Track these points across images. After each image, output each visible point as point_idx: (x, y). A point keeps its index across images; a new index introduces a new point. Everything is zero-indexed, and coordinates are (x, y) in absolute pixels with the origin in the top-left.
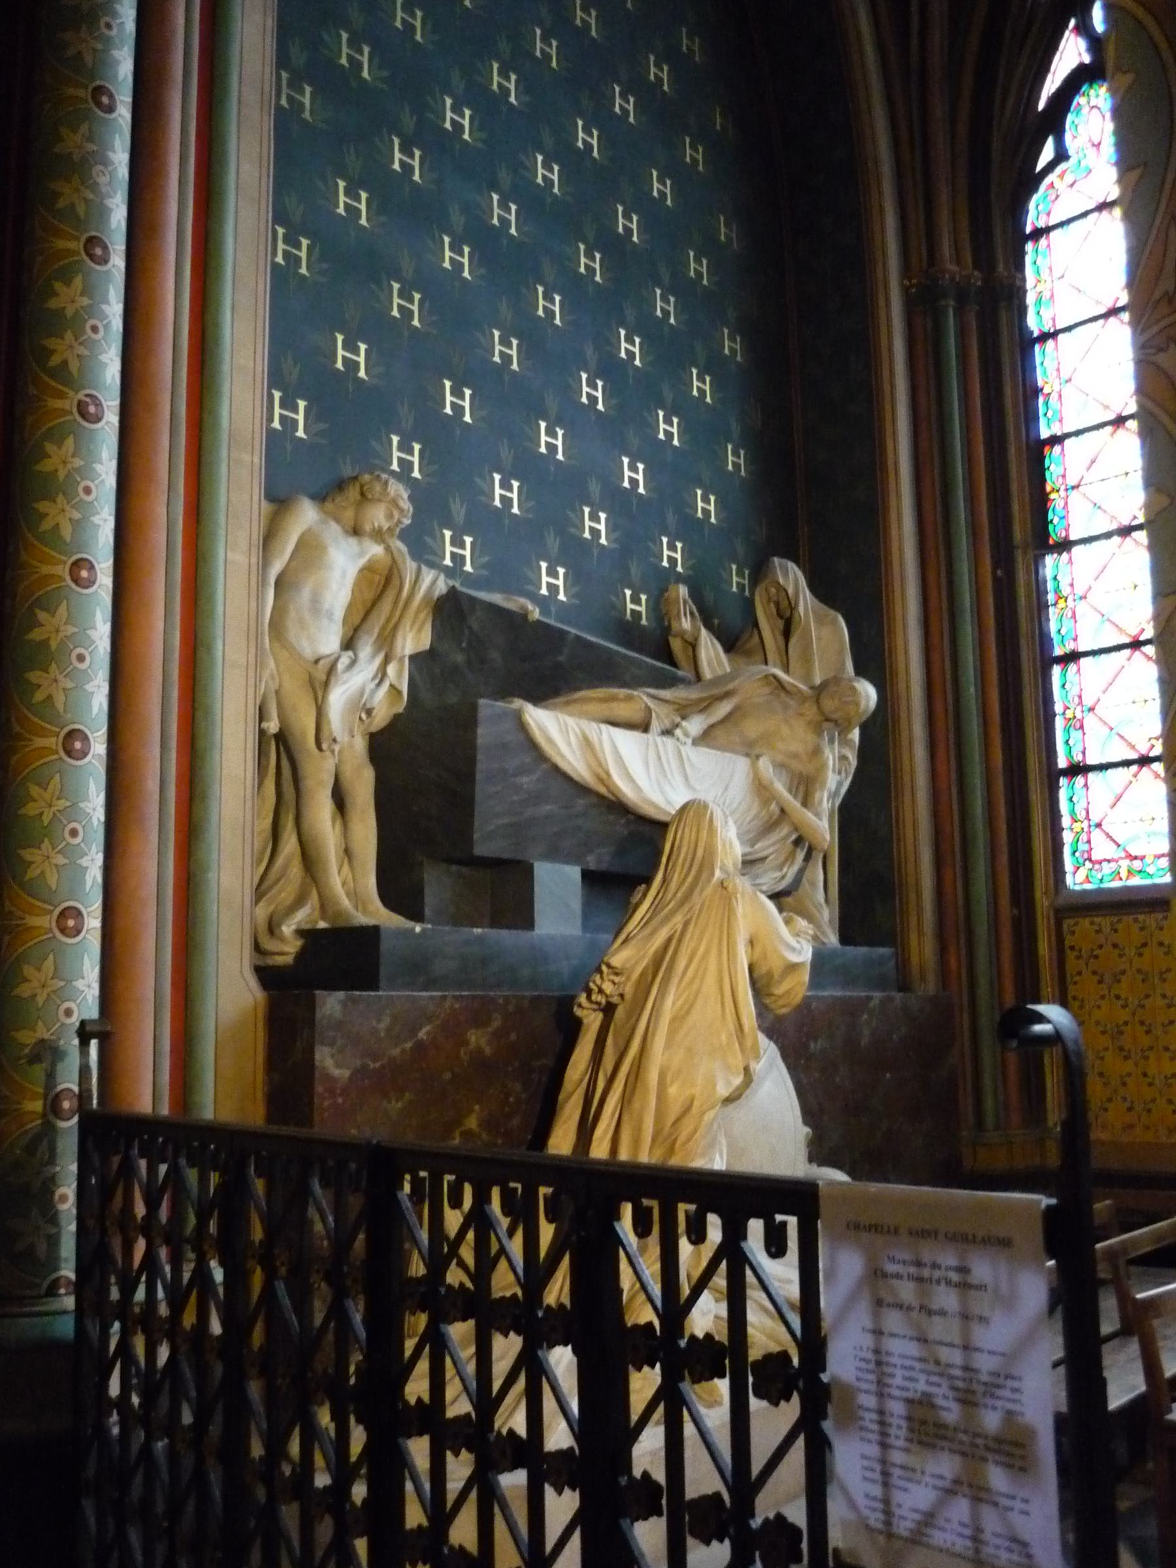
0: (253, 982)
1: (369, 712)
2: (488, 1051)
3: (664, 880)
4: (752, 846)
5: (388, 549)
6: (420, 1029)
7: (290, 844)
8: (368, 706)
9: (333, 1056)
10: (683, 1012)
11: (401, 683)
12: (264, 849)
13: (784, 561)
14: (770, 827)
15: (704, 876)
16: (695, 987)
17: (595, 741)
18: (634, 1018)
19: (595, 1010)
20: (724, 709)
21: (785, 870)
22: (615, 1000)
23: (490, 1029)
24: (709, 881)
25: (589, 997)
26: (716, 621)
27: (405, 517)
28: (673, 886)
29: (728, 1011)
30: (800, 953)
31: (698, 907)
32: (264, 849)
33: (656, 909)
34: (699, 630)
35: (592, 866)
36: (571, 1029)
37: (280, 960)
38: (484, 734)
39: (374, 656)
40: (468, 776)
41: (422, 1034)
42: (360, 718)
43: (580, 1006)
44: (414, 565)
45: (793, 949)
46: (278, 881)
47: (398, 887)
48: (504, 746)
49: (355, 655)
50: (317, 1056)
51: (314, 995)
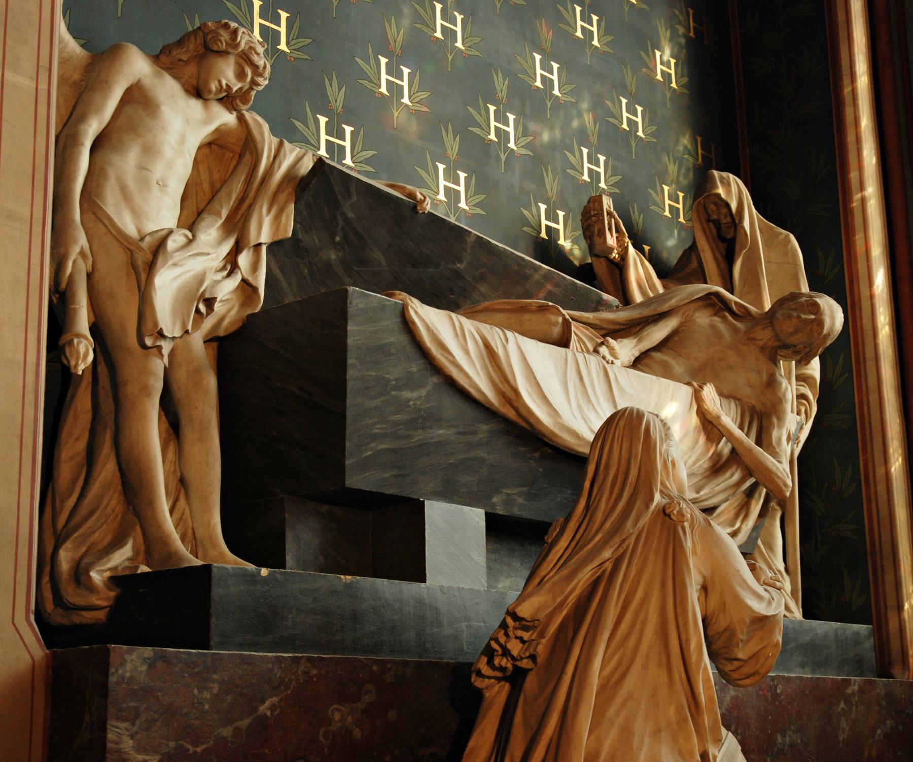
0: (31, 637)
1: (210, 302)
2: (357, 733)
3: (587, 507)
4: (698, 492)
5: (241, 118)
6: (263, 701)
7: (107, 469)
8: (207, 296)
9: (132, 737)
10: (614, 679)
11: (256, 278)
12: (74, 481)
13: (724, 174)
14: (717, 468)
15: (639, 504)
16: (631, 643)
17: (500, 352)
18: (549, 689)
19: (499, 679)
20: (658, 333)
21: (738, 525)
22: (525, 664)
23: (360, 705)
24: (647, 507)
25: (490, 663)
26: (647, 248)
27: (261, 75)
28: (599, 516)
29: (676, 677)
30: (769, 603)
31: (633, 539)
32: (74, 481)
33: (576, 546)
34: (627, 248)
35: (500, 510)
36: (470, 704)
37: (88, 617)
38: (357, 333)
39: (220, 242)
40: (337, 388)
41: (264, 709)
42: (198, 311)
43: (479, 673)
44: (275, 141)
45: (759, 597)
46: (91, 514)
47: (251, 526)
48: (383, 350)
49: (194, 236)
50: (110, 736)
51: (108, 651)
